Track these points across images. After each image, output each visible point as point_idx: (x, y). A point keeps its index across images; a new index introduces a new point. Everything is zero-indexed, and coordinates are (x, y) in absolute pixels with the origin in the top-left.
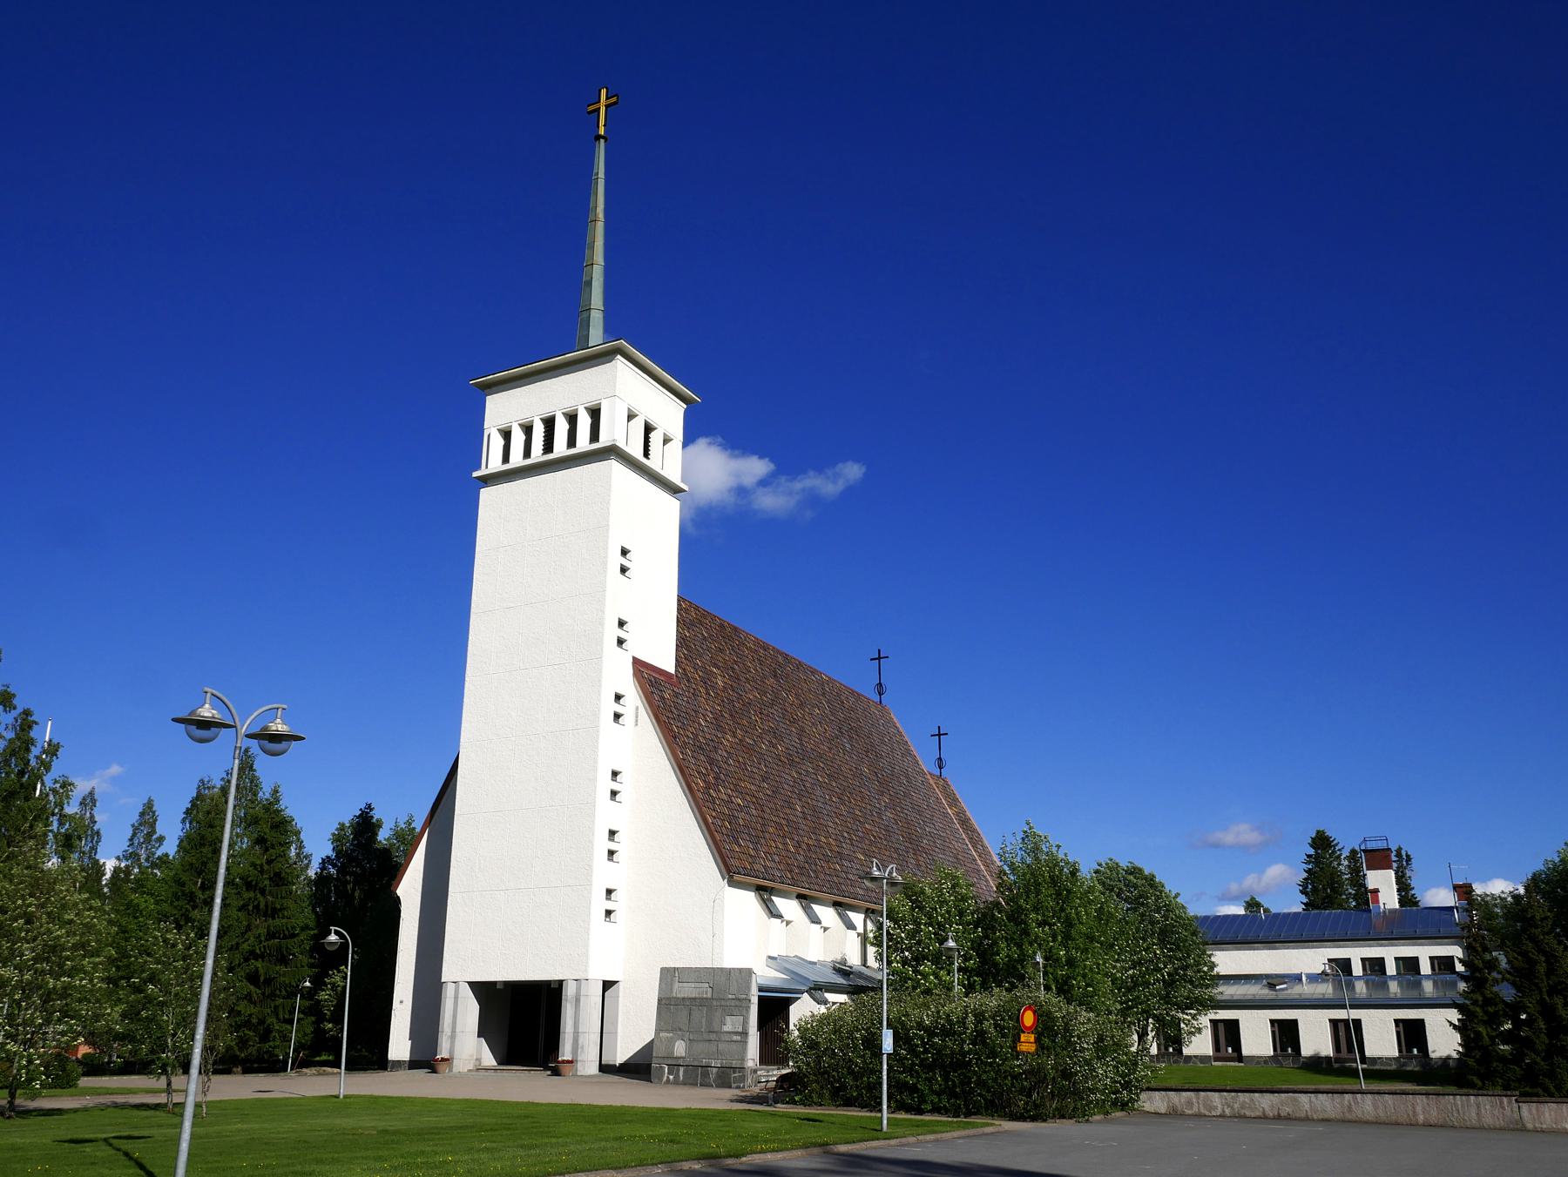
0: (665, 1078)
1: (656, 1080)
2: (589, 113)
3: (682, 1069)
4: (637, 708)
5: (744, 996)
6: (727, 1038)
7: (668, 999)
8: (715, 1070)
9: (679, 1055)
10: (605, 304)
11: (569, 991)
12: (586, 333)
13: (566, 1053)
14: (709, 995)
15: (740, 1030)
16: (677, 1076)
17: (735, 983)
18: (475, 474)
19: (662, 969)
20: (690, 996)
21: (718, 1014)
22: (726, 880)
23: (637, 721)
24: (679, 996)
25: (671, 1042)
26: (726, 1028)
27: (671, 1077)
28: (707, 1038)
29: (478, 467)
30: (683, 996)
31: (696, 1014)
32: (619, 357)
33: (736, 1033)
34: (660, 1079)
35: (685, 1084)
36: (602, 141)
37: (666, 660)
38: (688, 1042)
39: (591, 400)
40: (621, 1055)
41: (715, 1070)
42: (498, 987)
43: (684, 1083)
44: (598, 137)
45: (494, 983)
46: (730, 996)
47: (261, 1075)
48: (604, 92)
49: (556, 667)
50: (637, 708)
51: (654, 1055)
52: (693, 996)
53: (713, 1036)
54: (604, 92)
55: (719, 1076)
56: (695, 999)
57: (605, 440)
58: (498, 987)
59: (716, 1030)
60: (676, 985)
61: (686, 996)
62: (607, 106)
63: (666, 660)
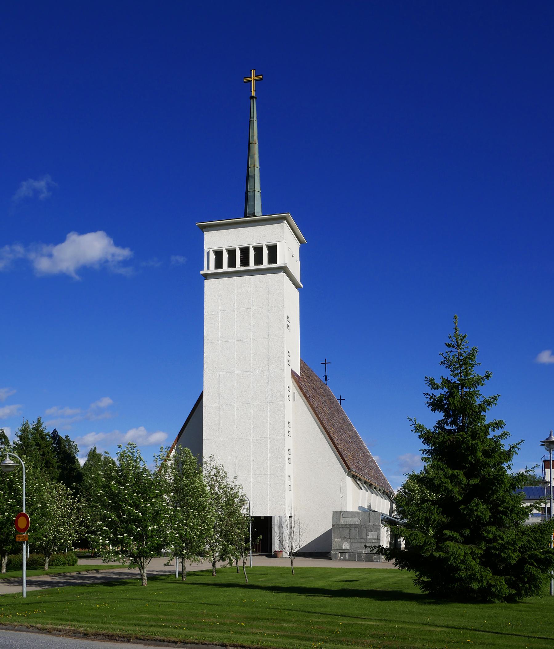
0: (339, 558)
1: (334, 559)
2: (245, 82)
3: (347, 555)
4: (294, 393)
5: (378, 524)
6: (370, 541)
7: (338, 525)
8: (364, 555)
9: (345, 548)
10: (261, 188)
11: (276, 521)
12: (254, 203)
13: (276, 547)
14: (359, 523)
15: (376, 538)
16: (345, 557)
17: (372, 518)
18: (202, 272)
19: (333, 512)
20: (349, 524)
21: (365, 531)
22: (347, 473)
23: (294, 399)
24: (343, 523)
25: (341, 543)
26: (369, 537)
27: (342, 558)
28: (360, 541)
29: (203, 269)
30: (345, 523)
31: (353, 531)
32: (285, 221)
33: (375, 539)
34: (336, 558)
35: (349, 560)
36: (254, 99)
37: (298, 372)
38: (350, 543)
39: (271, 242)
40: (295, 549)
41: (364, 555)
42: (261, 519)
43: (349, 560)
44: (252, 97)
45: (259, 517)
46: (370, 524)
47: (83, 559)
48: (253, 72)
49: (257, 372)
50: (294, 393)
51: (333, 548)
52: (351, 523)
53: (363, 541)
54: (253, 72)
55: (366, 557)
56: (352, 525)
57: (280, 262)
58: (261, 519)
59: (364, 538)
60: (342, 519)
61: (347, 523)
62: (256, 80)
63: (298, 372)
